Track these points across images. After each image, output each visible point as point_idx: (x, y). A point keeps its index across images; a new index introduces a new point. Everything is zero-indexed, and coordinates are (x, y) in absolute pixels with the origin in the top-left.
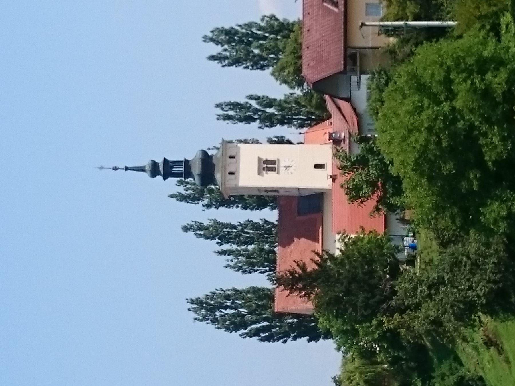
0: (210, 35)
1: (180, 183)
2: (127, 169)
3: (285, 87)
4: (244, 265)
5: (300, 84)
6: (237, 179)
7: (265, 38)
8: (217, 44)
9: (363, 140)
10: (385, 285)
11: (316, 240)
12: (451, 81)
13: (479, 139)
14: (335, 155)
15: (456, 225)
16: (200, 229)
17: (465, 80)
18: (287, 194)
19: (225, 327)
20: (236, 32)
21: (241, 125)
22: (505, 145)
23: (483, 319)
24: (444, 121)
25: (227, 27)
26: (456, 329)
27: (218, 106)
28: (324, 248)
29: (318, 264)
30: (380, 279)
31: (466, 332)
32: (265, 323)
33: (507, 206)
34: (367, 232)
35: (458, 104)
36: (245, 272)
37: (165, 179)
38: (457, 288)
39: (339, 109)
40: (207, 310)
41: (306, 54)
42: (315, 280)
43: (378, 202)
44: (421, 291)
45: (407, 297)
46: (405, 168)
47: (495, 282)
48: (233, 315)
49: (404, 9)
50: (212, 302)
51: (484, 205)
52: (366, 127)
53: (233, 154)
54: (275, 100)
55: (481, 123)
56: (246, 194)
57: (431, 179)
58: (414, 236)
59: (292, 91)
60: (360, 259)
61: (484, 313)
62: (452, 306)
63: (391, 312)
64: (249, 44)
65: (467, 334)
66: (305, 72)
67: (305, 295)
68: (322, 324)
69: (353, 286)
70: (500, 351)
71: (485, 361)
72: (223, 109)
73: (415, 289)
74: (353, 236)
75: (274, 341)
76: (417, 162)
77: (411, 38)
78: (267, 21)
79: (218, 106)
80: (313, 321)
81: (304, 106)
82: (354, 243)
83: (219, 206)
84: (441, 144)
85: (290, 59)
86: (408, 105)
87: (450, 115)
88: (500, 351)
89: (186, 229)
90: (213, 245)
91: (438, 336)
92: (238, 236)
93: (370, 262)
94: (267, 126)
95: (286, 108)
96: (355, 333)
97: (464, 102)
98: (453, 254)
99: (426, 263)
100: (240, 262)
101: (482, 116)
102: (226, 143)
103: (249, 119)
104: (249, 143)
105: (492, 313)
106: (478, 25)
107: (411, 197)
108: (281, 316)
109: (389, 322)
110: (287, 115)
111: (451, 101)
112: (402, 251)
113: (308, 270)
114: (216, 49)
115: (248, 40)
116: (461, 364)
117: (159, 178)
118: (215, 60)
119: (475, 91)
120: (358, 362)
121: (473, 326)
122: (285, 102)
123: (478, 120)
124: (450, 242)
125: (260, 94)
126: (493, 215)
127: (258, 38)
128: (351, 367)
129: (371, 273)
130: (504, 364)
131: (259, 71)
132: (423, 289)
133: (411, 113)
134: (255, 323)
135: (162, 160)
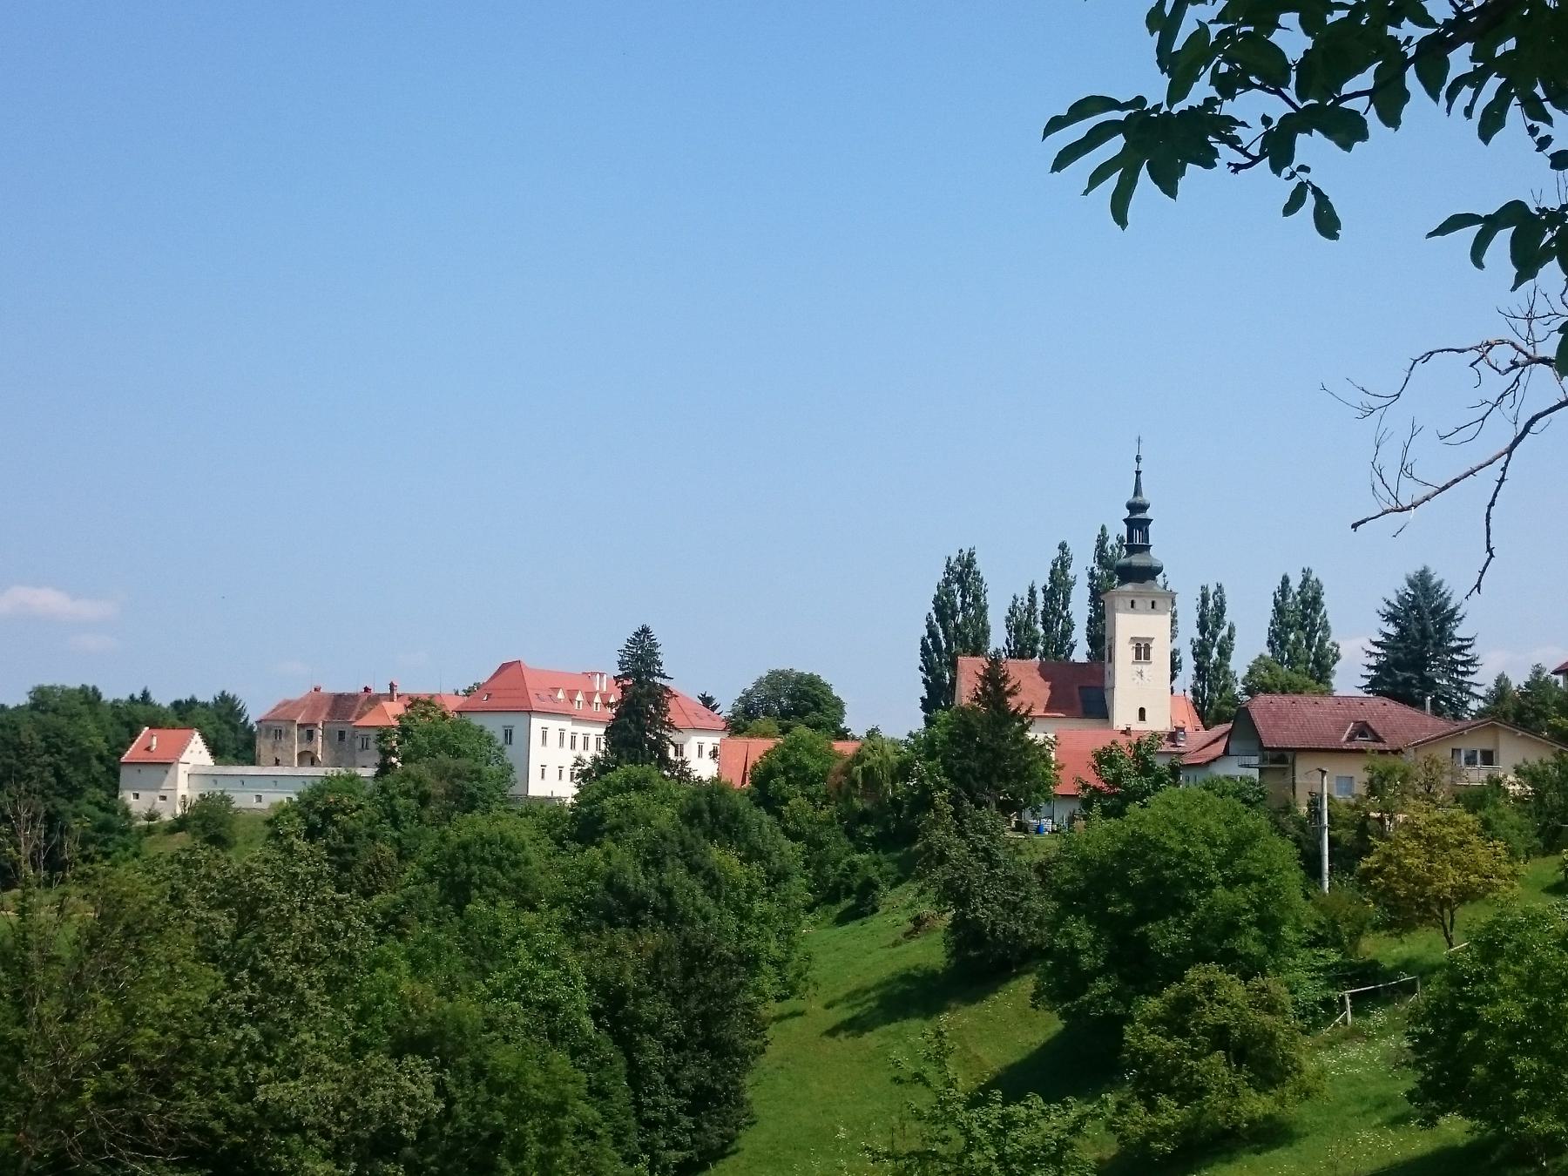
0: (1313, 578)
1: (1121, 540)
2: (1138, 473)
3: (1246, 672)
4: (1017, 619)
5: (1249, 691)
6: (1126, 611)
7: (1309, 647)
8: (1300, 587)
9: (1175, 771)
10: (989, 795)
11: (1048, 709)
12: (1247, 884)
13: (1174, 916)
14: (1154, 734)
15: (1063, 884)
16: (1062, 564)
17: (1249, 901)
18: (1106, 673)
19: (939, 596)
20: (1317, 611)
21: (1196, 617)
22: (1166, 949)
23: (948, 914)
24: (1196, 873)
25: (1324, 599)
26: (933, 881)
27: (1219, 587)
28: (1036, 719)
29: (1015, 711)
30: (998, 789)
31: (931, 893)
32: (944, 645)
33: (1088, 949)
34: (1057, 772)
35: (1219, 891)
36: (1008, 619)
37: (1125, 520)
38: (985, 884)
39: (1216, 741)
40: (960, 574)
41: (1285, 700)
42: (996, 707)
43: (1094, 787)
44: (981, 839)
45: (973, 821)
46: (1136, 823)
47: (993, 931)
48: (954, 604)
49: (1345, 825)
50: (970, 579)
51: (1089, 921)
52: (1191, 774)
53: (1157, 606)
54: (1229, 659)
55: (1195, 919)
56: (1107, 621)
57: (1121, 854)
58: (1053, 831)
59: (1240, 680)
60: (1022, 764)
61: (955, 917)
62: (962, 878)
63: (955, 801)
64: (1302, 628)
65: (928, 895)
66: (1262, 698)
67: (977, 694)
68: (942, 715)
69: (989, 755)
70: (909, 935)
71: (897, 916)
72: (1215, 593)
73: (984, 832)
74: (1053, 755)
75: (922, 655)
76: (1142, 837)
77: (1306, 834)
78: (1331, 650)
79: (1219, 587)
80: (947, 702)
81: (1220, 695)
82: (1044, 757)
83: (1091, 589)
84: (1167, 869)
85: (1282, 679)
86: (1218, 829)
87: (1205, 880)
88: (909, 935)
89: (1063, 547)
90: (1043, 580)
91: (926, 860)
92: (1055, 612)
93: (1019, 776)
94: (1194, 649)
95: (1218, 673)
96: (931, 756)
97: (1221, 899)
98: (1028, 880)
99: (1016, 846)
100: (1021, 614)
101: (1204, 921)
102: (1172, 598)
103: (1202, 626)
104: (1172, 626)
105: (958, 924)
106: (1323, 919)
107: (498, 978)
108: (953, 665)
109: (943, 798)
110: (1209, 675)
111: (1223, 883)
112: (1033, 815)
113: (1009, 699)
114: (1295, 585)
115: (1306, 626)
116: (893, 886)
117: (1127, 513)
118: (1283, 584)
119: (1237, 913)
120: (894, 758)
121: (938, 903)
122: (1226, 672)
123: (1198, 915)
124: (1044, 876)
125: (1236, 641)
126: (1076, 931)
127: (1310, 637)
128: (888, 749)
129: (1006, 778)
130: (893, 940)
131: (1266, 639)
132: (985, 841)
133: (1206, 832)
134: (945, 632)
135: (1150, 518)
